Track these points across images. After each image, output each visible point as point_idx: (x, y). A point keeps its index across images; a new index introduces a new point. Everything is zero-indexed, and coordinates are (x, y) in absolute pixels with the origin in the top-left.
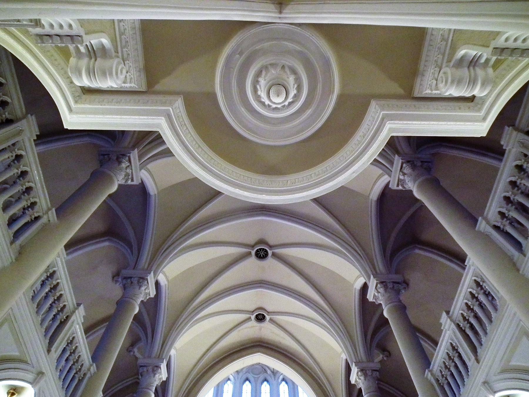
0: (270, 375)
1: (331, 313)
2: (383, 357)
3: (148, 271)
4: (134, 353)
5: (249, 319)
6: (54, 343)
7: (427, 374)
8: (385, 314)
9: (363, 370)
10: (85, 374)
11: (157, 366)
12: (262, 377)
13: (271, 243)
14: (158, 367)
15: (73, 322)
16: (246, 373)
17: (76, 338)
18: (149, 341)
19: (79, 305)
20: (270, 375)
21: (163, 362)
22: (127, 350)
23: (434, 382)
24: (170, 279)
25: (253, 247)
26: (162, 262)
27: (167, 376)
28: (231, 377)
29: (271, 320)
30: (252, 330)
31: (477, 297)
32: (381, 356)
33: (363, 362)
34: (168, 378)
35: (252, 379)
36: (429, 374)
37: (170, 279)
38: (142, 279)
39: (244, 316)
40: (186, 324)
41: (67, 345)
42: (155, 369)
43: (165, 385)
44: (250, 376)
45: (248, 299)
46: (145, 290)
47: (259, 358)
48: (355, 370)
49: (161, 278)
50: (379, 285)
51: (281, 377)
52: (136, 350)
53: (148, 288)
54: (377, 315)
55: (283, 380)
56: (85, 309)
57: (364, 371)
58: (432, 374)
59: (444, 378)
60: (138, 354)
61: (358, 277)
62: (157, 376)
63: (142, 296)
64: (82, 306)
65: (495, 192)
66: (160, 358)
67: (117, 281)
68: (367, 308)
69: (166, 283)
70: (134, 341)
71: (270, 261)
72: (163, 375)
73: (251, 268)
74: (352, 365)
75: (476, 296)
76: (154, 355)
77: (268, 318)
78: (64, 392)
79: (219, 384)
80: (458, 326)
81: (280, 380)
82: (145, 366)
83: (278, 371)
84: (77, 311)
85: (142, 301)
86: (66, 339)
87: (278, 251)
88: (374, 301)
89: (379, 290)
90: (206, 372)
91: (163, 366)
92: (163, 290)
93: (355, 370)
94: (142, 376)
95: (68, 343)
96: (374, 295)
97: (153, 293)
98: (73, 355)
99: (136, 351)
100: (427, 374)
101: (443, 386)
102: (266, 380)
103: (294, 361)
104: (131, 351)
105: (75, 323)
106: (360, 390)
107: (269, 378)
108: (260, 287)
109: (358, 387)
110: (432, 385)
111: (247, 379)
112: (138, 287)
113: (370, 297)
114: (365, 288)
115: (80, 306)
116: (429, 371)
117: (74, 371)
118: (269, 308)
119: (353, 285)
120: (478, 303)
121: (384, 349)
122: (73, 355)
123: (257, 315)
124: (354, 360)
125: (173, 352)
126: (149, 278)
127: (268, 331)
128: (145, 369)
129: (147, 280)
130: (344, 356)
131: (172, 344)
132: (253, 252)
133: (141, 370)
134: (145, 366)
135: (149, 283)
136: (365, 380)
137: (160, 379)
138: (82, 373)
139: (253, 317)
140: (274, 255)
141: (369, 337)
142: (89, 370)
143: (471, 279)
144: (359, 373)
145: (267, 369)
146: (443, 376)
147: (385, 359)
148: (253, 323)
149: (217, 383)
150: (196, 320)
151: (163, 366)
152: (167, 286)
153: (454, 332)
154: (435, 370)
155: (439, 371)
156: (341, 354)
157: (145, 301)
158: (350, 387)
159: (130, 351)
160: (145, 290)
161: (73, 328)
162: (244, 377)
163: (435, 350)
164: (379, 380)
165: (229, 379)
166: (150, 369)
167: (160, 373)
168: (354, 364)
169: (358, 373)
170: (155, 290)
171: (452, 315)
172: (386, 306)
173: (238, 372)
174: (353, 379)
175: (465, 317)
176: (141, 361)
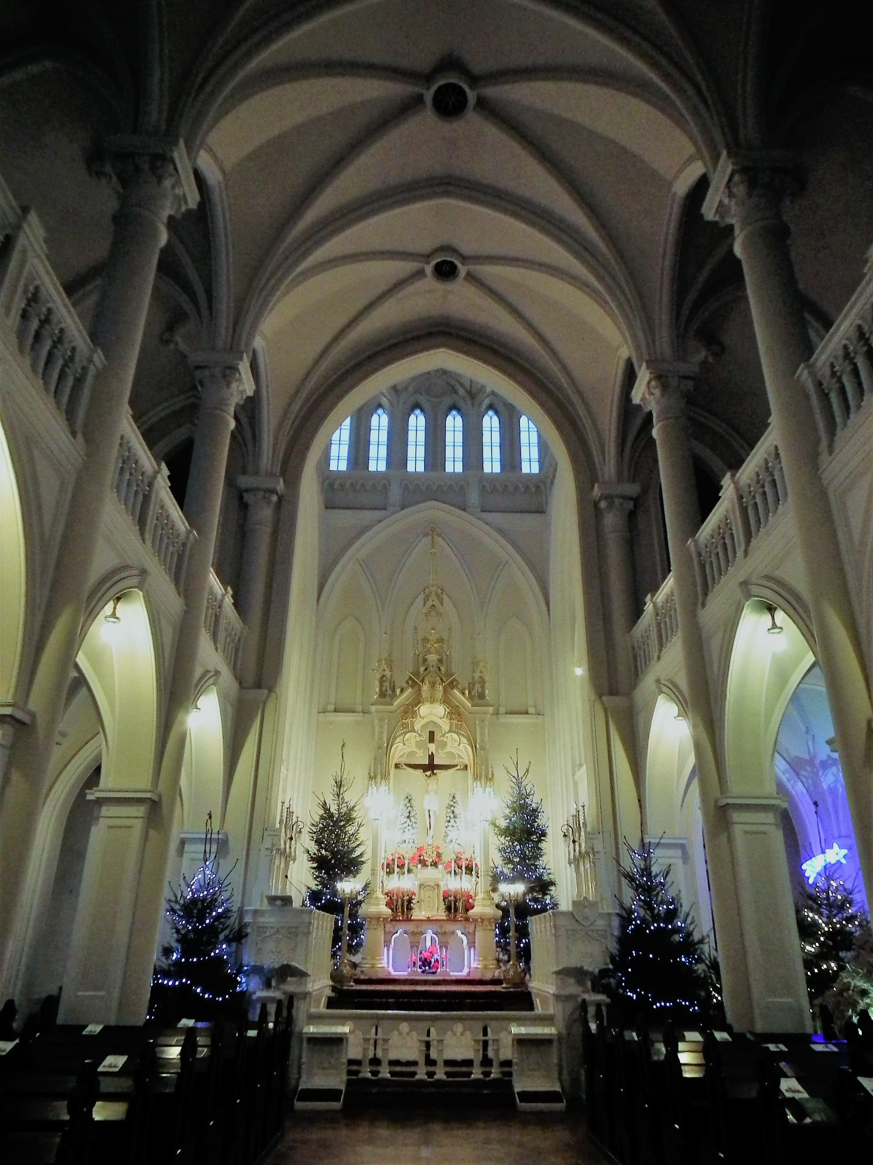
0: (463, 398)
1: (609, 256)
2: (706, 358)
3: (170, 135)
4: (177, 344)
5: (419, 274)
6: (19, 674)
7: (802, 373)
8: (738, 250)
9: (660, 378)
10: (85, 369)
11: (230, 368)
12: (447, 401)
13: (478, 66)
14: (234, 369)
15: (24, 252)
16: (415, 392)
17: (43, 290)
18: (205, 313)
19: (25, 210)
20: (463, 398)
21: (241, 359)
22: (161, 339)
23: (694, 555)
24: (228, 167)
25: (428, 78)
26: (200, 115)
27: (254, 387)
28: (384, 401)
29: (471, 277)
30: (426, 298)
31: (868, 339)
32: (703, 353)
33: (664, 360)
34: (257, 391)
35: (425, 405)
36: (806, 372)
37: (228, 166)
38: (160, 162)
39: (409, 267)
40: (276, 287)
41: (28, 305)
42: (228, 372)
43: (250, 409)
44: (422, 399)
45: (417, 224)
46: (173, 187)
47: (442, 359)
48: (644, 375)
49: (204, 161)
50: (737, 178)
51: (487, 402)
52: (178, 338)
53: (178, 183)
54: (721, 252)
55: (491, 407)
56: (41, 216)
57: (663, 379)
58: (812, 374)
59: (835, 380)
60: (182, 346)
61: (690, 160)
62: (234, 385)
63: (168, 203)
64: (33, 217)
65: (861, 294)
66: (235, 349)
67: (100, 174)
68: (697, 235)
69: (220, 177)
70: (171, 320)
71: (472, 121)
72: (245, 385)
73: (421, 142)
74: (640, 367)
75: (852, 355)
76: (220, 343)
77: (462, 270)
78: (53, 400)
79: (363, 407)
80: (741, 497)
81: (484, 407)
82: (205, 367)
83: (483, 387)
84: (25, 226)
85: (171, 218)
86: (20, 290)
87: (491, 91)
88: (717, 219)
89: (735, 190)
90: (331, 388)
91: (244, 366)
92: (216, 198)
93: (644, 375)
94: (202, 385)
95: (29, 300)
96: (721, 204)
97: (193, 199)
98: (47, 326)
99: (179, 340)
100: (802, 373)
101: (746, 507)
102: (454, 407)
103: (515, 363)
104: (171, 341)
105: (30, 254)
106: (650, 414)
107: (461, 404)
108: (447, 194)
109: (646, 410)
110: (691, 559)
111: (417, 406)
112: (154, 180)
113: (709, 211)
114: (701, 186)
115: (29, 212)
116: (807, 366)
117: (60, 362)
118: (466, 249)
119: (671, 185)
120: (866, 348)
121: (711, 337)
122: (47, 326)
123: (438, 264)
124: (647, 358)
125: (258, 343)
126: (176, 155)
127: (461, 300)
128: (207, 372)
129: (173, 161)
130: (625, 352)
131: (254, 327)
132: (429, 97)
133: (198, 374)
134: (205, 367)
135: (179, 169)
136: (663, 396)
137: (242, 392)
138: (77, 366)
139: (429, 269)
140: (482, 104)
141: (685, 312)
142: (90, 360)
143: (840, 342)
144: (653, 383)
145: (458, 387)
146: (834, 374)
147: (711, 359)
148: (430, 282)
149: (358, 406)
150: (303, 273)
151: (244, 366)
152: (223, 185)
153: (734, 506)
154: (819, 364)
155: (828, 364)
156: (619, 347)
157: (179, 216)
158: (627, 410)
159: (167, 342)
160: (173, 187)
161: (28, 266)
162: (412, 400)
163: (822, 338)
164: (690, 399)
165: (380, 406)
166: (217, 371)
167: (240, 380)
168: (644, 364)
169: (649, 383)
170: (197, 191)
171: (814, 363)
172: (742, 230)
173: (395, 389)
174: (637, 396)
175: (849, 354)
176: (195, 358)
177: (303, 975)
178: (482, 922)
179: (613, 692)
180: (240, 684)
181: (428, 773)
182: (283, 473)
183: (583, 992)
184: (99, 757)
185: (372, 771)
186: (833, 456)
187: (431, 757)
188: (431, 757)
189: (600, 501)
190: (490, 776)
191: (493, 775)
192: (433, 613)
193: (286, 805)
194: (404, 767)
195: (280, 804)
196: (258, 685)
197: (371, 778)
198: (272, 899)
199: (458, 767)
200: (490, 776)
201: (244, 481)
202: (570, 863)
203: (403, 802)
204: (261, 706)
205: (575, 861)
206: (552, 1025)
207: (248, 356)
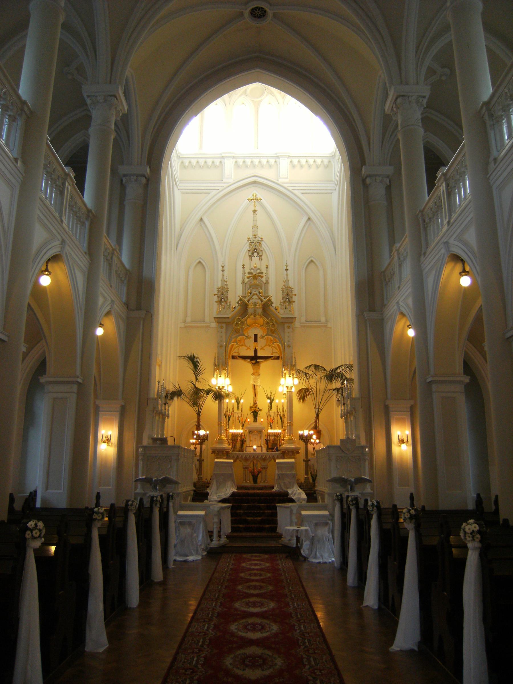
139: (247, 13)
177: (176, 483)
178: (288, 454)
179: (372, 309)
180: (128, 308)
181: (254, 362)
182: (149, 163)
183: (345, 491)
184: (44, 352)
185: (216, 361)
186: (497, 165)
187: (256, 351)
188: (256, 351)
189: (366, 178)
190: (294, 363)
191: (295, 363)
192: (255, 254)
193: (161, 384)
194: (238, 357)
195: (157, 383)
196: (139, 308)
197: (215, 365)
198: (155, 440)
199: (274, 358)
200: (294, 363)
201: (123, 170)
202: (342, 417)
203: (316, 408)
204: (142, 322)
205: (346, 416)
206: (326, 510)
207: (122, 87)
